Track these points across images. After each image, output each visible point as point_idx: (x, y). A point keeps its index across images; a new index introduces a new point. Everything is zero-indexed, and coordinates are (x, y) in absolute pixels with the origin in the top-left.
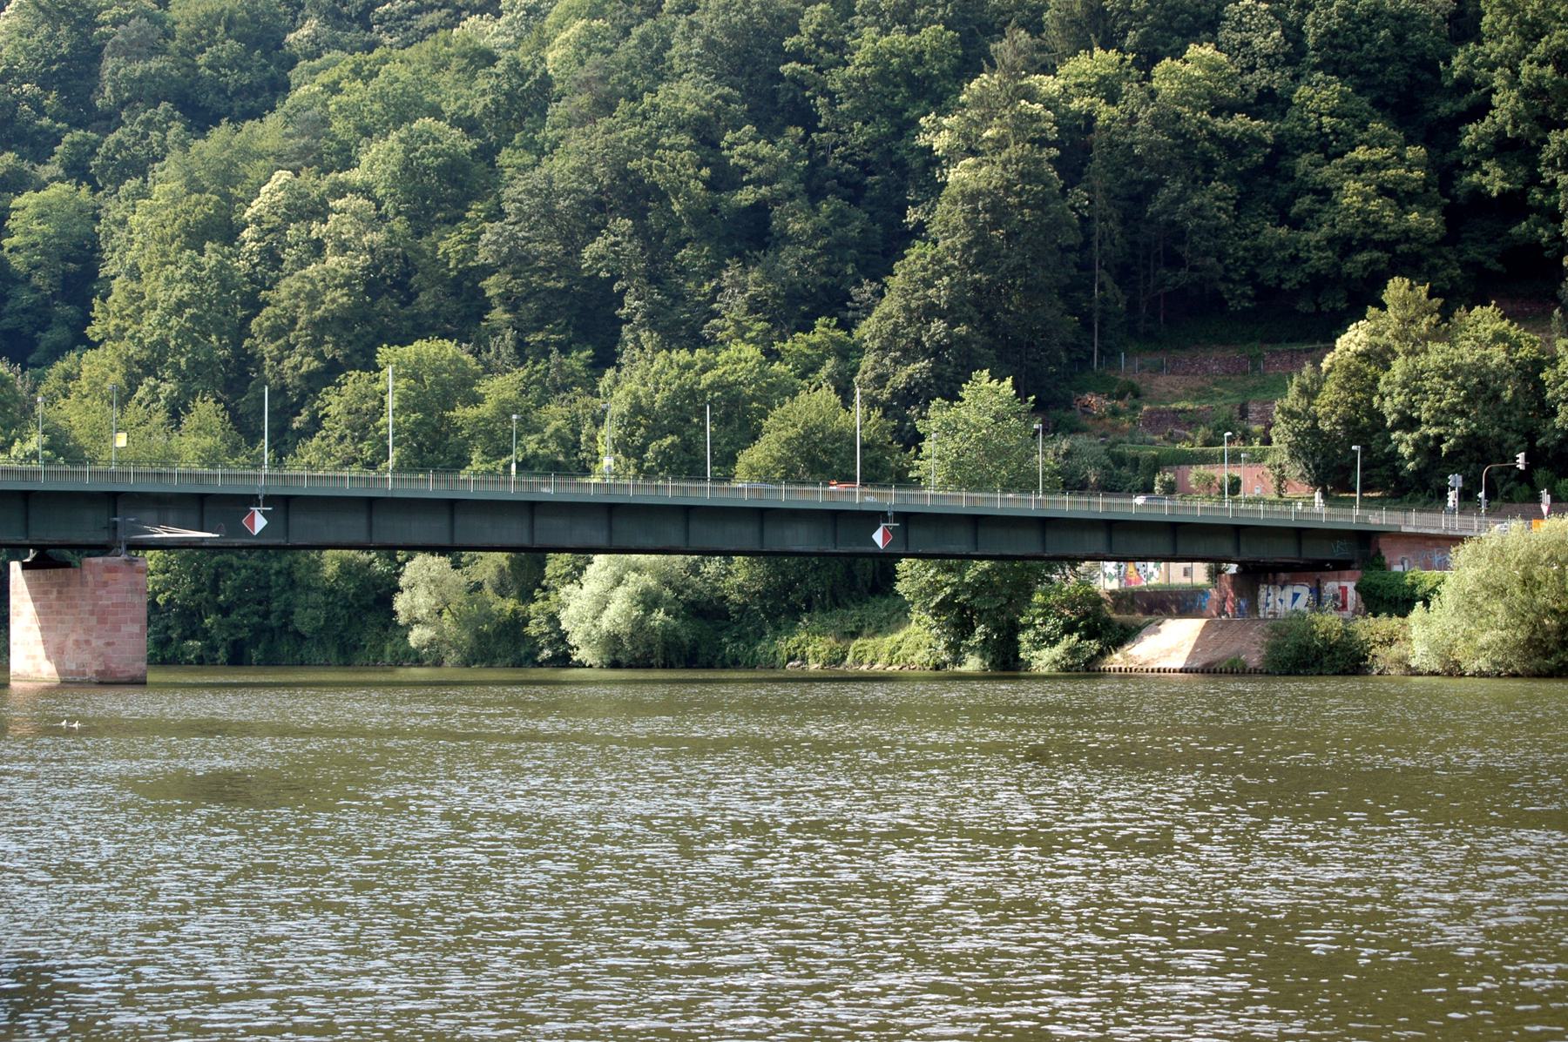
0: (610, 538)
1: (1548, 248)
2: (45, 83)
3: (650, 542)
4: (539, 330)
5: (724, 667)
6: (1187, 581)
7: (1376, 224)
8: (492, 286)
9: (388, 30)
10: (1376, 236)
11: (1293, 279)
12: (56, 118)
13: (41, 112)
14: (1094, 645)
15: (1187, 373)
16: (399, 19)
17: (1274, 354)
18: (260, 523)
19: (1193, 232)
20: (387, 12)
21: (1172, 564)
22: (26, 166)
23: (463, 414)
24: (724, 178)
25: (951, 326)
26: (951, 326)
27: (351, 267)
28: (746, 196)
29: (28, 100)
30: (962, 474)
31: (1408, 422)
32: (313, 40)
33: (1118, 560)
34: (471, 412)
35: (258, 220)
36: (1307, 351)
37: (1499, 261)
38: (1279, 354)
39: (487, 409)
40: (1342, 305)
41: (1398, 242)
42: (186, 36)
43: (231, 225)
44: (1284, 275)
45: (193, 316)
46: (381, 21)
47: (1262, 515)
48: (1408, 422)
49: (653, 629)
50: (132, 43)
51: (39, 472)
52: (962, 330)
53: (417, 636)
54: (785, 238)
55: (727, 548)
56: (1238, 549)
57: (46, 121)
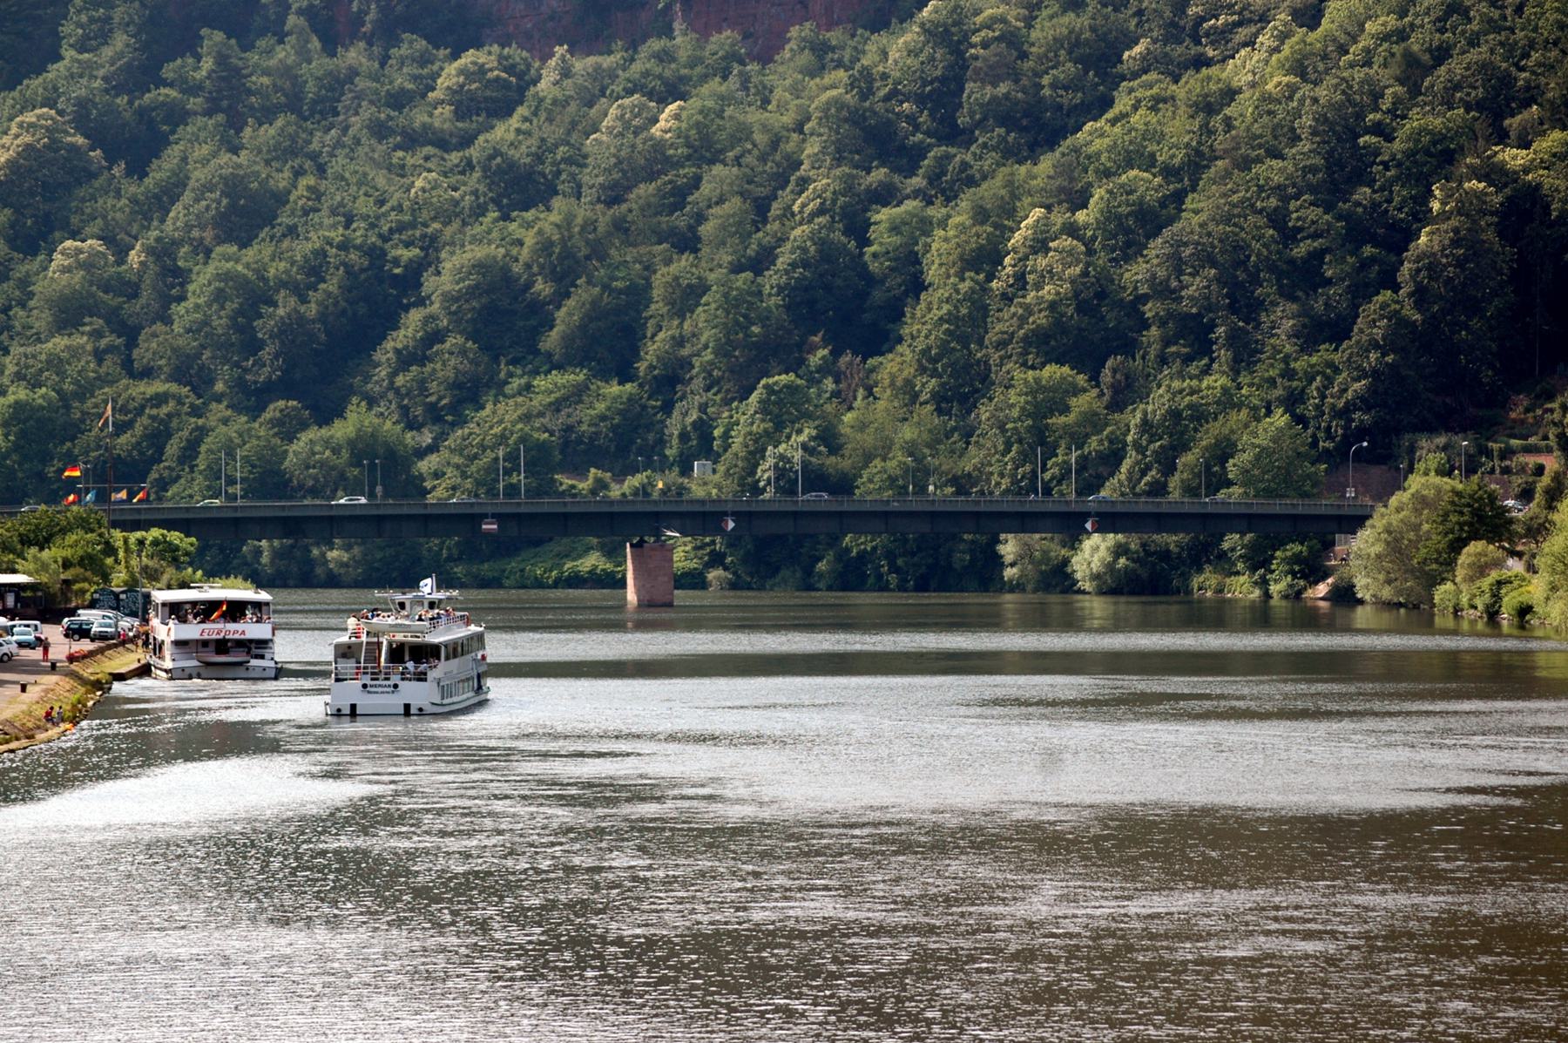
2: (921, 100)
4: (1176, 343)
8: (1150, 310)
9: (1212, 43)
12: (928, 133)
13: (917, 127)
14: (1302, 583)
16: (1223, 32)
18: (731, 525)
20: (1211, 27)
22: (896, 178)
23: (1058, 420)
24: (1290, 236)
25: (1384, 355)
26: (1384, 355)
27: (1058, 293)
28: (1301, 250)
29: (907, 116)
30: (1190, 490)
32: (1144, 58)
34: (1063, 419)
35: (1015, 250)
39: (1070, 418)
42: (1039, 57)
43: (998, 252)
45: (947, 330)
46: (1207, 35)
49: (1119, 570)
50: (990, 67)
52: (1389, 359)
53: (1009, 573)
54: (1329, 282)
57: (920, 136)
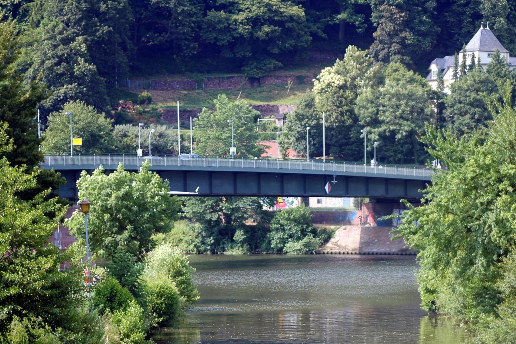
0: (235, 189)
1: (359, 28)
3: (314, 194)
5: (354, 259)
6: (319, 206)
7: (276, 11)
10: (276, 18)
11: (225, 39)
15: (163, 90)
17: (209, 79)
19: (180, 14)
21: (328, 198)
31: (375, 122)
33: (355, 197)
36: (228, 78)
37: (324, 32)
38: (212, 79)
40: (249, 54)
41: (286, 21)
44: (220, 37)
47: (277, 168)
48: (375, 122)
51: (190, 161)
55: (272, 194)
56: (406, 191)
